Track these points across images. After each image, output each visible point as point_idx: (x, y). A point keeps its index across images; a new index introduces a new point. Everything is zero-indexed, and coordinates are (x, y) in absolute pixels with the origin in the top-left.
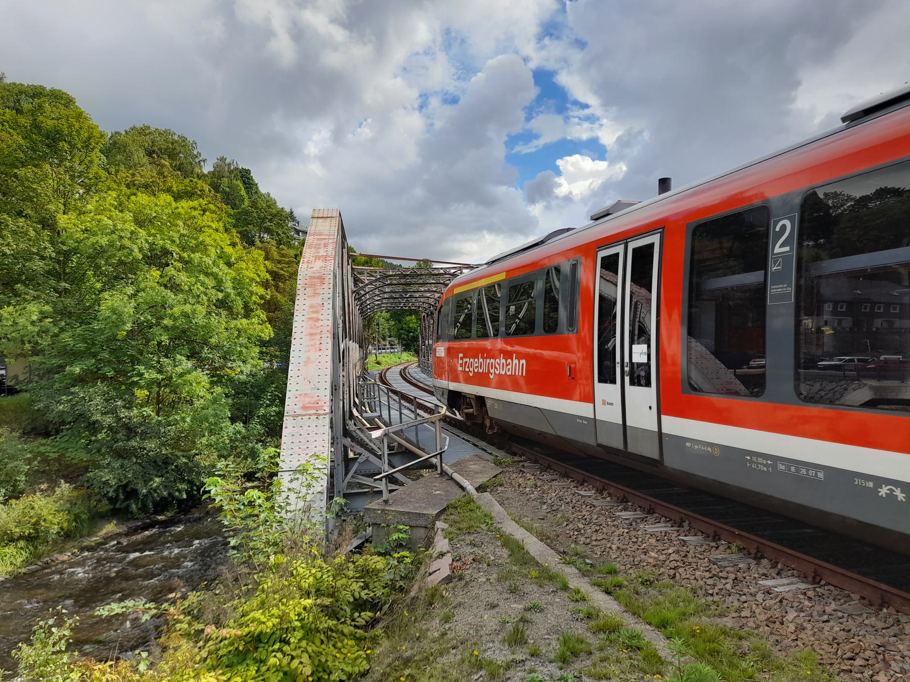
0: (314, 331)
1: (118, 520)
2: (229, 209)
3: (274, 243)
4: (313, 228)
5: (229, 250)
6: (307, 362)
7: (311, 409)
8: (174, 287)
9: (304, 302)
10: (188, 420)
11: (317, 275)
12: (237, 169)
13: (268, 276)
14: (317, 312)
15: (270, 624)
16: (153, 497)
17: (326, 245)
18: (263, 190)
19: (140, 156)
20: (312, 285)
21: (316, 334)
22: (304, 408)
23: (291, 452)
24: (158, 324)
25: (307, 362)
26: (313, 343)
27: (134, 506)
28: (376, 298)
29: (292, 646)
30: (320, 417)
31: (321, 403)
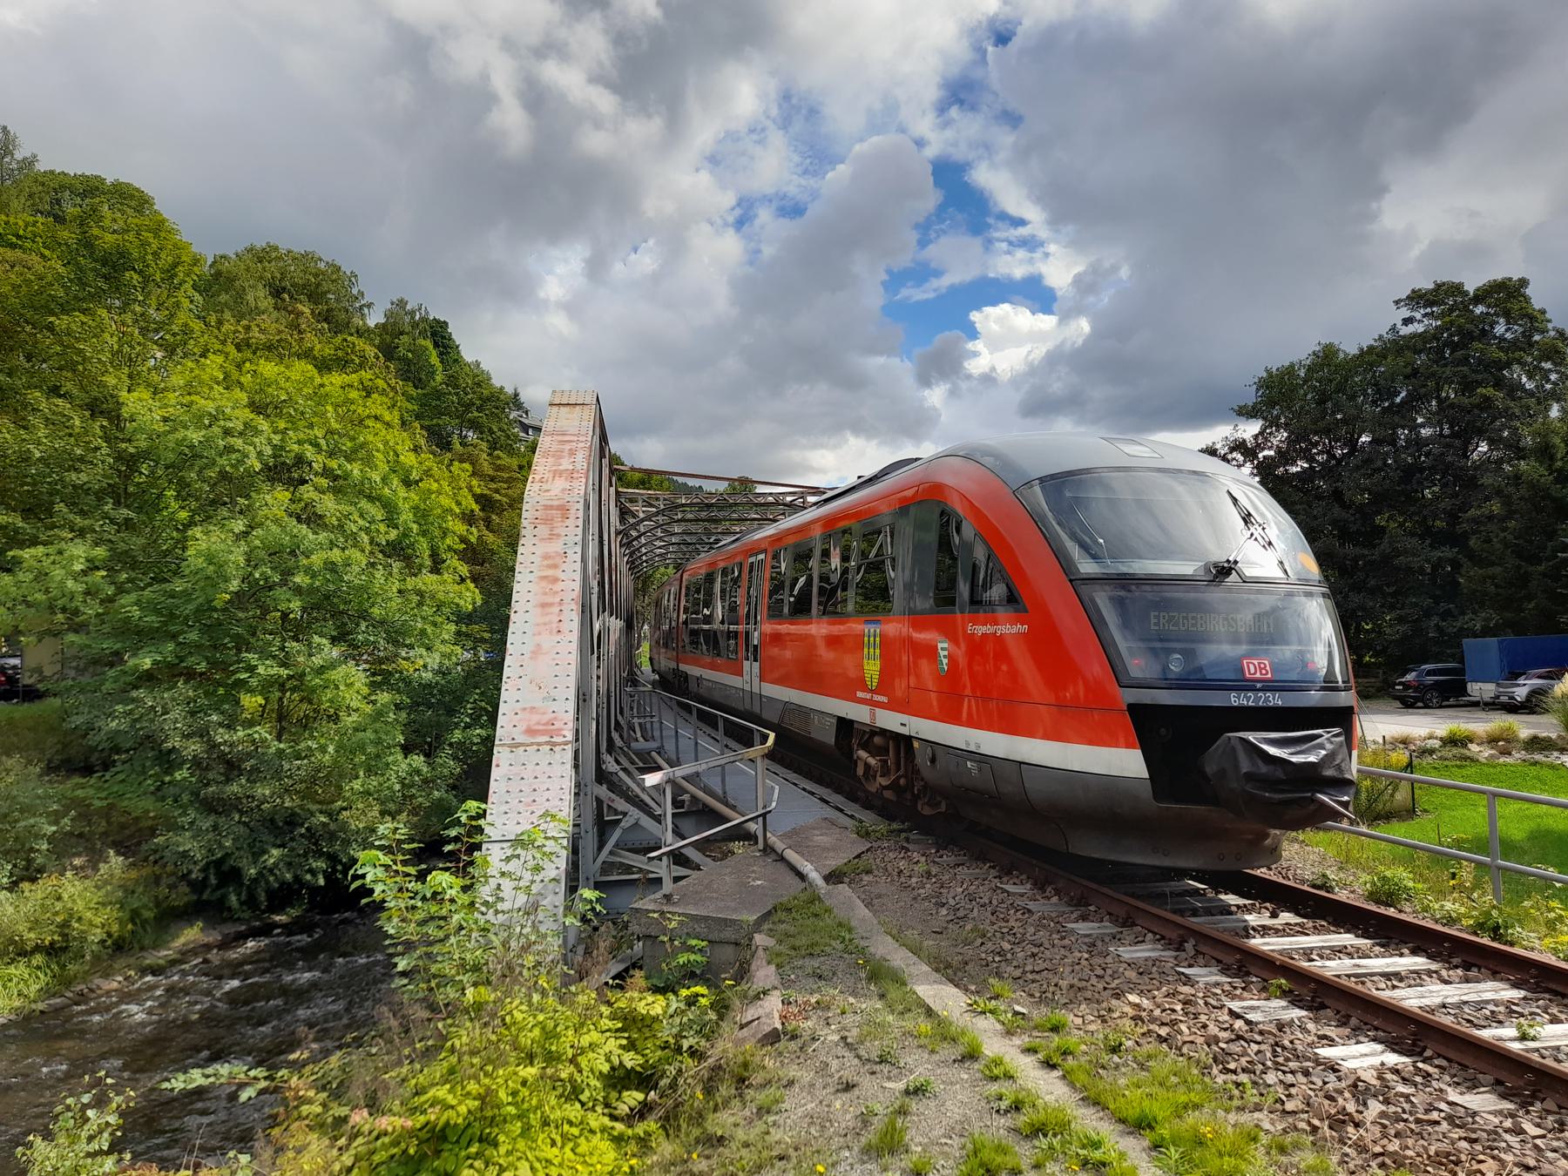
0: (549, 600)
1: (205, 921)
2: (413, 392)
3: (484, 445)
4: (552, 423)
5: (409, 459)
6: (537, 652)
7: (542, 734)
8: (312, 519)
9: (533, 549)
10: (331, 749)
11: (556, 503)
13: (475, 507)
14: (555, 566)
15: (463, 1109)
16: (267, 882)
17: (572, 453)
18: (468, 355)
19: (259, 297)
20: (547, 521)
21: (551, 605)
22: (530, 732)
23: (505, 808)
24: (284, 583)
25: (537, 652)
26: (547, 619)
27: (233, 898)
29: (502, 1150)
30: (557, 749)
31: (558, 725)
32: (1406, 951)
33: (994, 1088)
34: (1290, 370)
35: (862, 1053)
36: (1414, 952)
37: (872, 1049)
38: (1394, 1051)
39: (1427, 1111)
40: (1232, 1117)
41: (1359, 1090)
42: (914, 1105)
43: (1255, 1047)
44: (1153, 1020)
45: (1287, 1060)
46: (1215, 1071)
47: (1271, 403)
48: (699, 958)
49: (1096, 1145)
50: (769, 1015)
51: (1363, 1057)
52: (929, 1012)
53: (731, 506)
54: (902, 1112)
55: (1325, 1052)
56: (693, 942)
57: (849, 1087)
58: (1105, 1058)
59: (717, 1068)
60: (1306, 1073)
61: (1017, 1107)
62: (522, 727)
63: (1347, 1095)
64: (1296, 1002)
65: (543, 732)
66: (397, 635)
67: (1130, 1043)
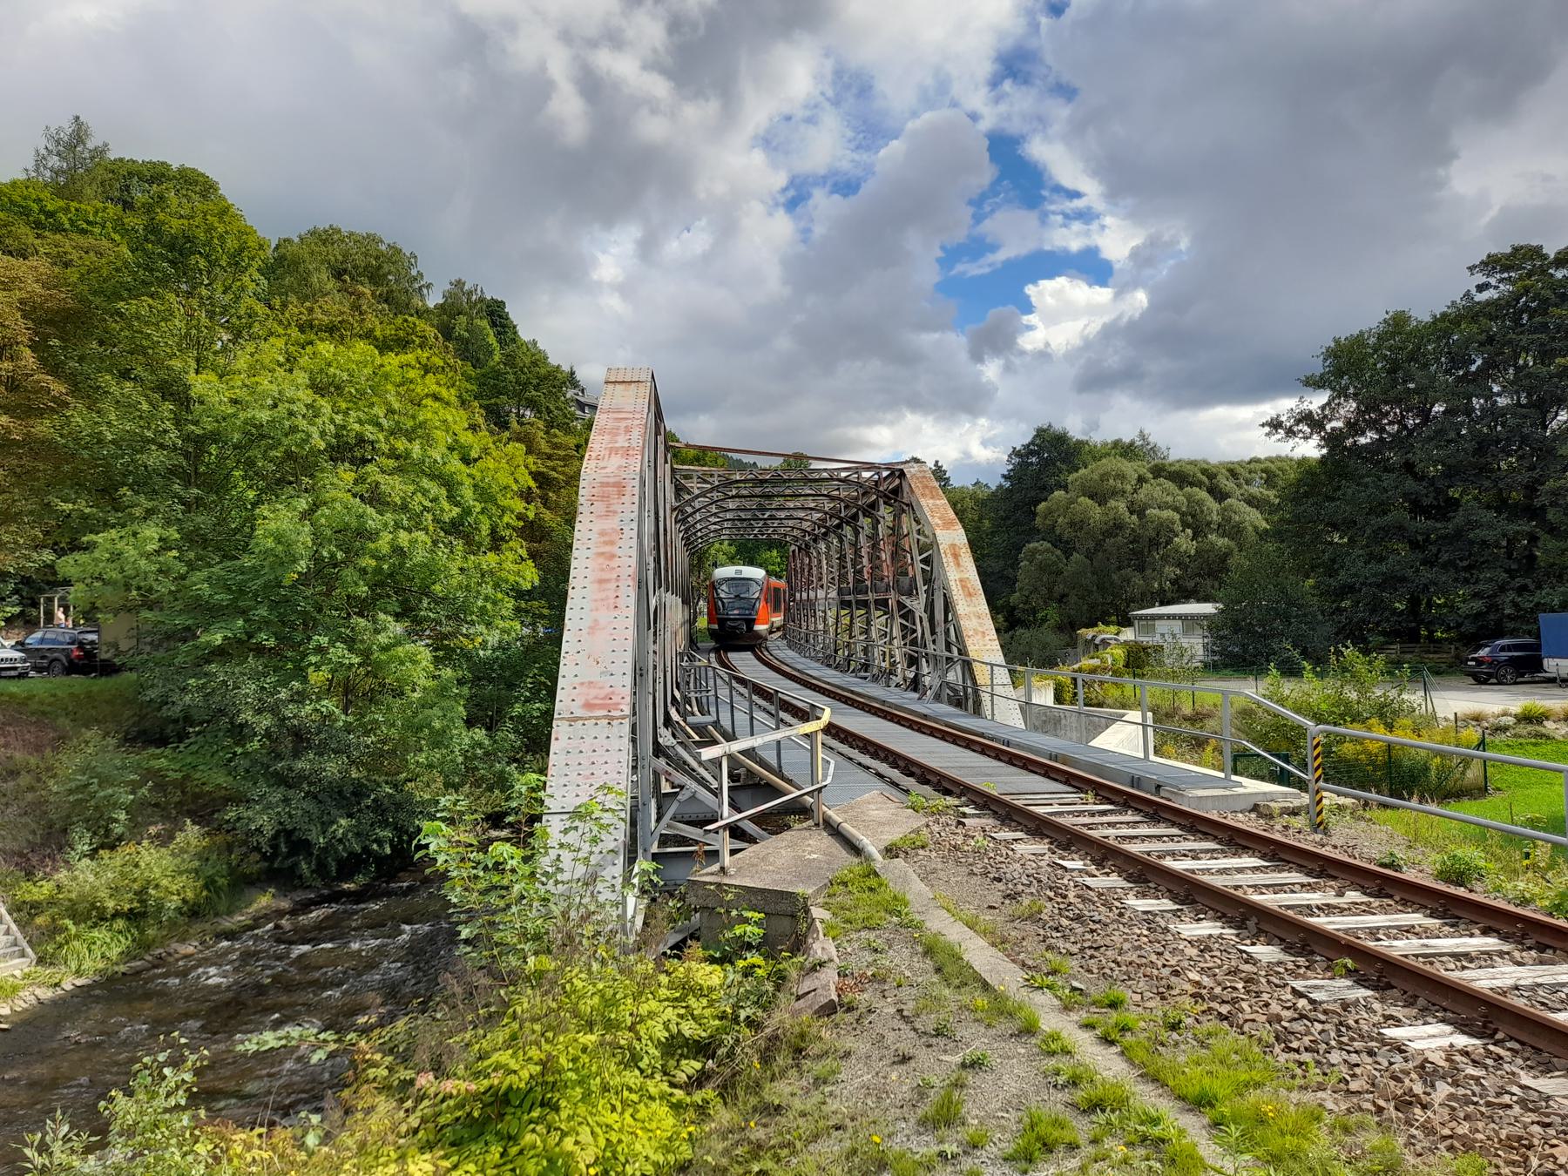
0: (606, 576)
2: (469, 369)
3: (541, 424)
4: (607, 401)
5: (467, 438)
6: (594, 627)
7: (599, 709)
8: (375, 498)
9: (591, 526)
11: (612, 480)
12: (482, 300)
13: (532, 484)
14: (612, 543)
15: (525, 1074)
17: (628, 430)
19: (322, 278)
20: (605, 498)
21: (608, 581)
22: (588, 706)
23: (564, 780)
25: (594, 627)
26: (603, 595)
28: (713, 519)
29: (564, 1114)
30: (615, 723)
31: (616, 699)
32: (1477, 932)
33: (1052, 1063)
34: (1359, 340)
35: (918, 1026)
36: (1485, 932)
37: (928, 1022)
38: (1464, 1033)
39: (1498, 1095)
40: (1295, 1096)
41: (1428, 1072)
42: (970, 1078)
43: (1319, 1026)
44: (1214, 998)
45: (1352, 1039)
46: (1277, 1049)
47: (1339, 373)
48: (756, 930)
49: (1155, 1121)
50: (826, 987)
51: (1431, 1038)
52: (986, 986)
53: (785, 481)
54: (959, 1085)
55: (1391, 1032)
56: (749, 914)
57: (905, 1059)
58: (1164, 1035)
59: (774, 1038)
60: (1371, 1053)
61: (1074, 1082)
63: (1414, 1076)
64: (1362, 982)
65: (601, 707)
66: (459, 614)
67: (1189, 1021)
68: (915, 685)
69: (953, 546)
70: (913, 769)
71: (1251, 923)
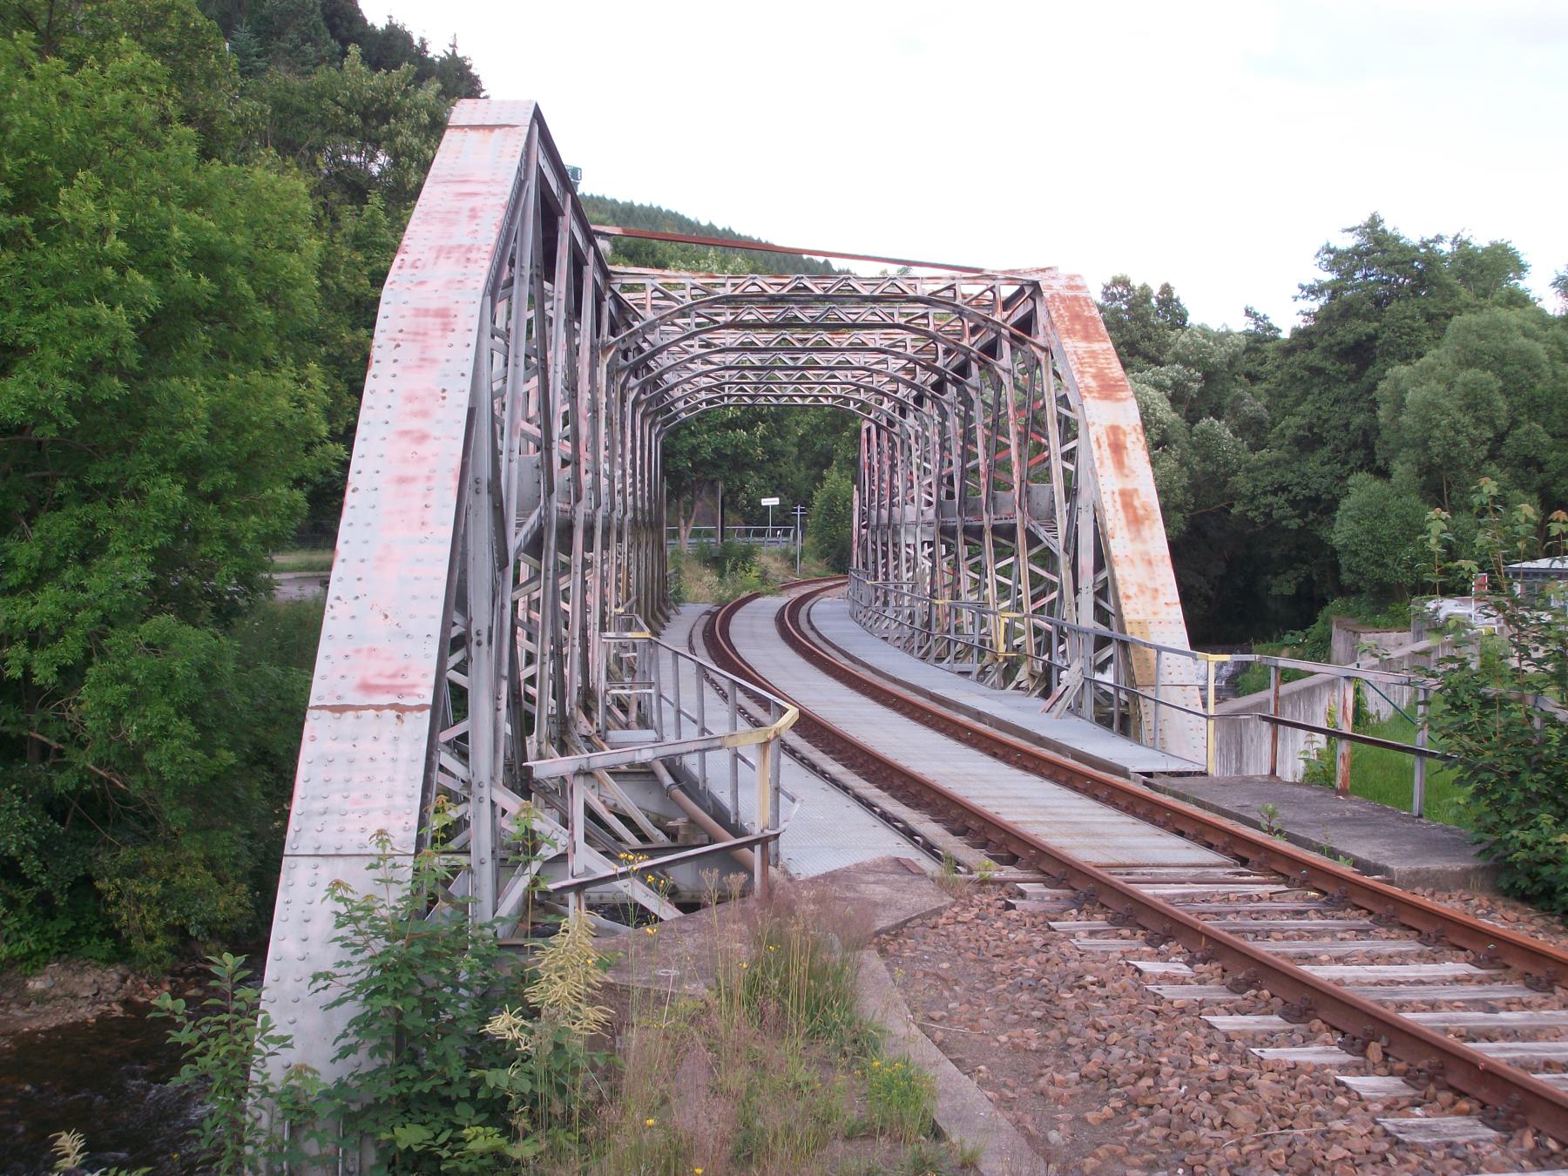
0: (410, 471)
14: (424, 414)
20: (419, 335)
28: (699, 367)
30: (408, 716)
62: (355, 678)
65: (388, 689)
68: (1045, 684)
69: (1115, 430)
70: (972, 823)
71: (1375, 1051)
